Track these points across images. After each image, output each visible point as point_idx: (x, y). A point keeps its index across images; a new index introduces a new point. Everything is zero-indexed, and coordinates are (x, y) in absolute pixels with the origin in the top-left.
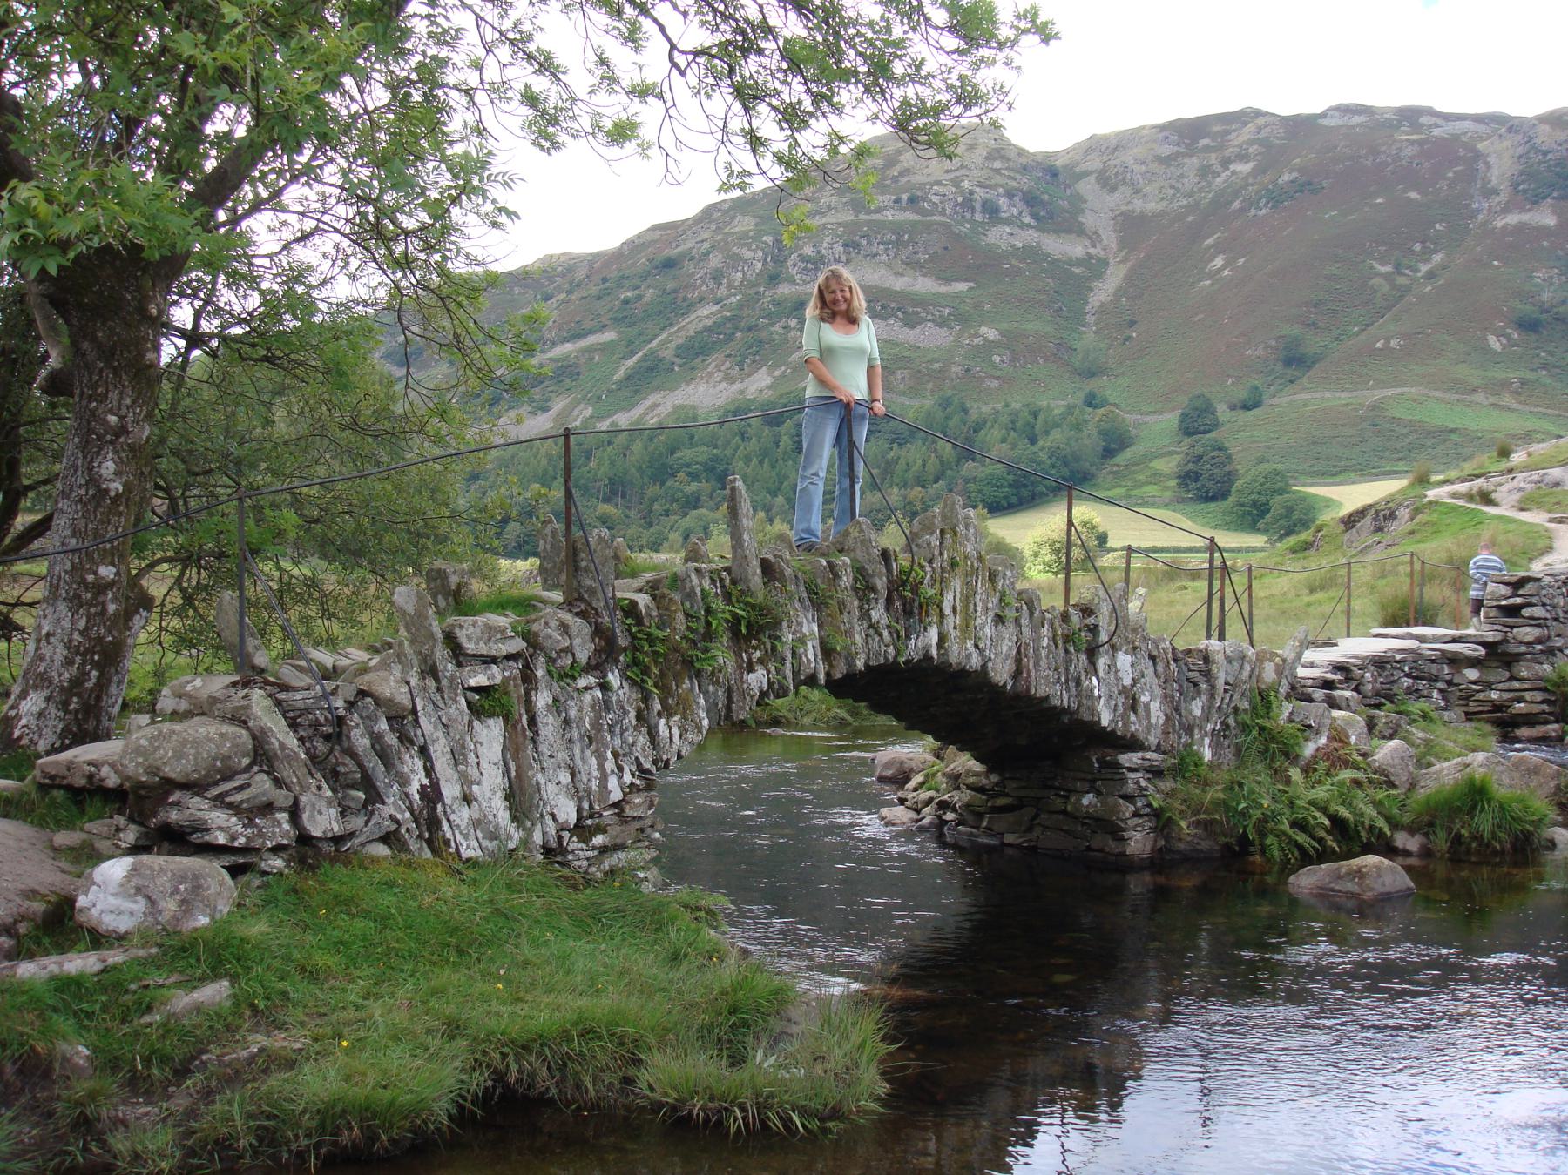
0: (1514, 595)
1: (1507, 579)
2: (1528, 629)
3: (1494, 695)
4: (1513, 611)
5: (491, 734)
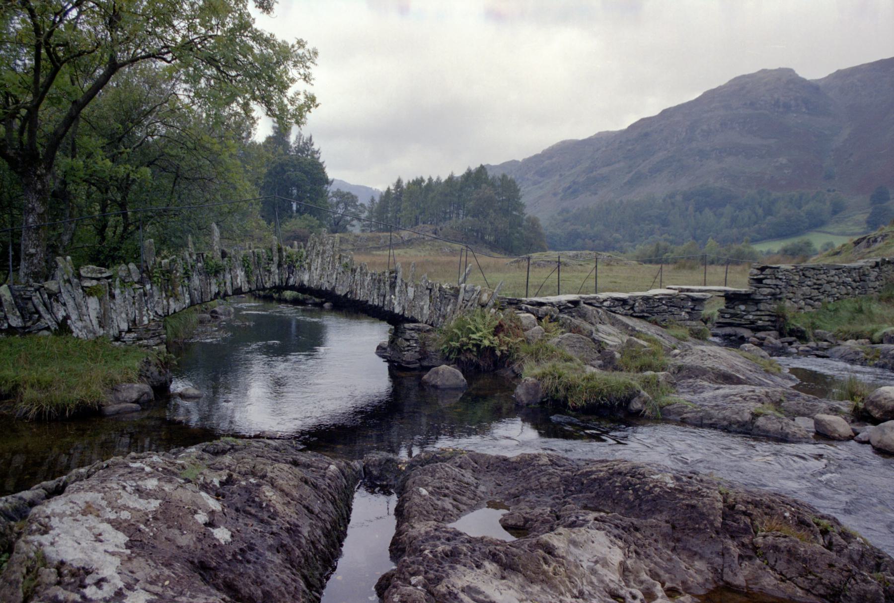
0: (761, 274)
1: (757, 267)
2: (765, 289)
3: (751, 317)
4: (760, 281)
5: (93, 303)
